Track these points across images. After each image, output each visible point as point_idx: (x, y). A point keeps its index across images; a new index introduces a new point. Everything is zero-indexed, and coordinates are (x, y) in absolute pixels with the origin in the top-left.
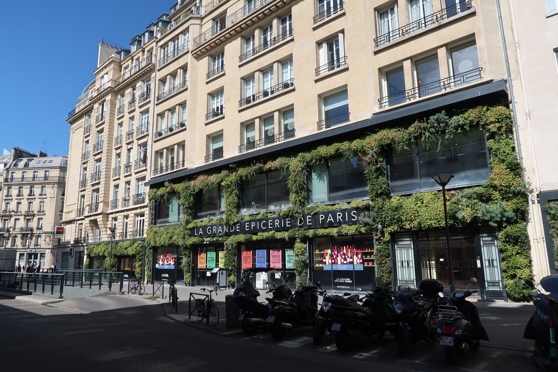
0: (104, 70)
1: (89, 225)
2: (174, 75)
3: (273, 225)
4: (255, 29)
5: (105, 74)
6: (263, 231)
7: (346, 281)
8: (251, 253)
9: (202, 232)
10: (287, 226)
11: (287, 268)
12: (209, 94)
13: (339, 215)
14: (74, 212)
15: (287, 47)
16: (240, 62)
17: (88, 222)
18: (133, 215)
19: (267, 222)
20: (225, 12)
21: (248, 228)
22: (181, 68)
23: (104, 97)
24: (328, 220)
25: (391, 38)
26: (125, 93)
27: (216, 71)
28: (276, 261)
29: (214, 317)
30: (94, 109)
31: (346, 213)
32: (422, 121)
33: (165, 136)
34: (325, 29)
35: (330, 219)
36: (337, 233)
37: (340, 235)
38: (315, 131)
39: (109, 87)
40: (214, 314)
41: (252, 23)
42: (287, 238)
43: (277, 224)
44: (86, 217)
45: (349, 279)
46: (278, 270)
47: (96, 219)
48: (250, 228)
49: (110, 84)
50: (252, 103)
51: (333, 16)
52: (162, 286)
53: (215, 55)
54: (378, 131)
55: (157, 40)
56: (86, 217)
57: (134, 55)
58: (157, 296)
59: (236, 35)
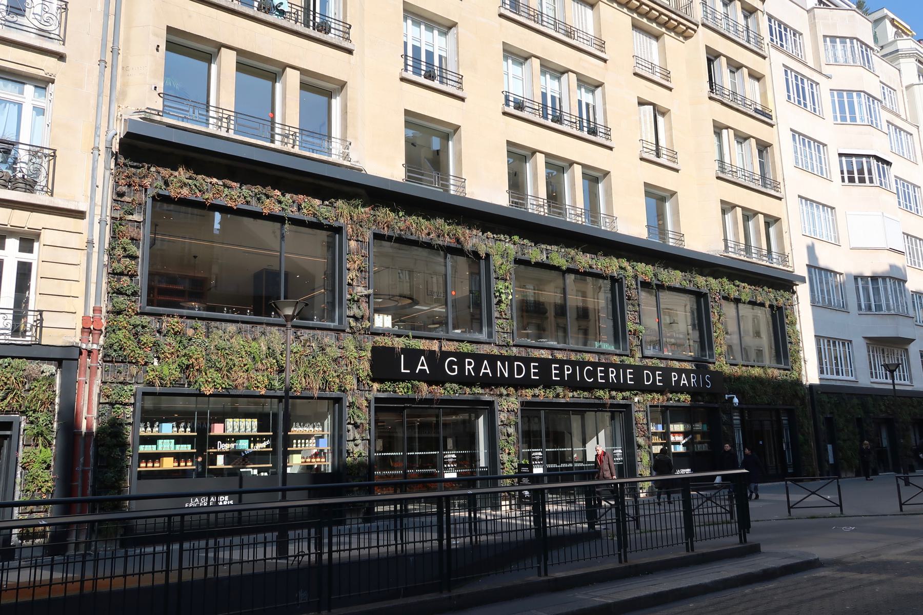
9: (686, 382)
10: (403, 371)
19: (595, 371)
21: (556, 375)
24: (419, 367)
43: (470, 367)
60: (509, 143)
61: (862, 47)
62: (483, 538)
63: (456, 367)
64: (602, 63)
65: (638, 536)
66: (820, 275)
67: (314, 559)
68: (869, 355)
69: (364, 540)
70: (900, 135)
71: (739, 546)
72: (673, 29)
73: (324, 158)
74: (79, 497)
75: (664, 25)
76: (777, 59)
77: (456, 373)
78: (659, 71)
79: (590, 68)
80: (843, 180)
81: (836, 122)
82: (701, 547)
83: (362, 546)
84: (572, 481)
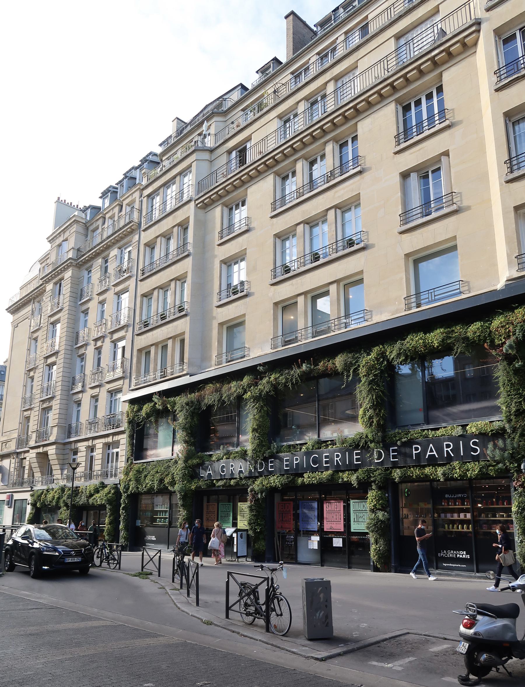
0: (62, 236)
1: (35, 460)
2: (167, 236)
4: (296, 161)
5: (63, 241)
6: (314, 470)
7: (458, 556)
8: (341, 505)
11: (352, 530)
12: (277, 236)
13: (338, 456)
14: (14, 441)
15: (351, 184)
16: (274, 211)
17: (34, 455)
18: (101, 446)
20: (249, 139)
22: (179, 225)
23: (61, 273)
24: (428, 453)
25: (515, 167)
26: (109, 256)
27: (351, 164)
28: (334, 520)
29: (279, 617)
30: (47, 291)
31: (461, 442)
33: (154, 326)
34: (414, 152)
35: (432, 451)
37: (448, 479)
38: (400, 312)
39: (70, 259)
40: (279, 613)
41: (257, 174)
42: (355, 484)
44: (32, 448)
45: (465, 552)
46: (338, 534)
47: (47, 451)
49: (70, 255)
50: (240, 295)
51: (427, 133)
52: (159, 554)
54: (517, 308)
55: (142, 188)
56: (32, 448)
57: (107, 211)
58: (148, 571)
59: (265, 171)
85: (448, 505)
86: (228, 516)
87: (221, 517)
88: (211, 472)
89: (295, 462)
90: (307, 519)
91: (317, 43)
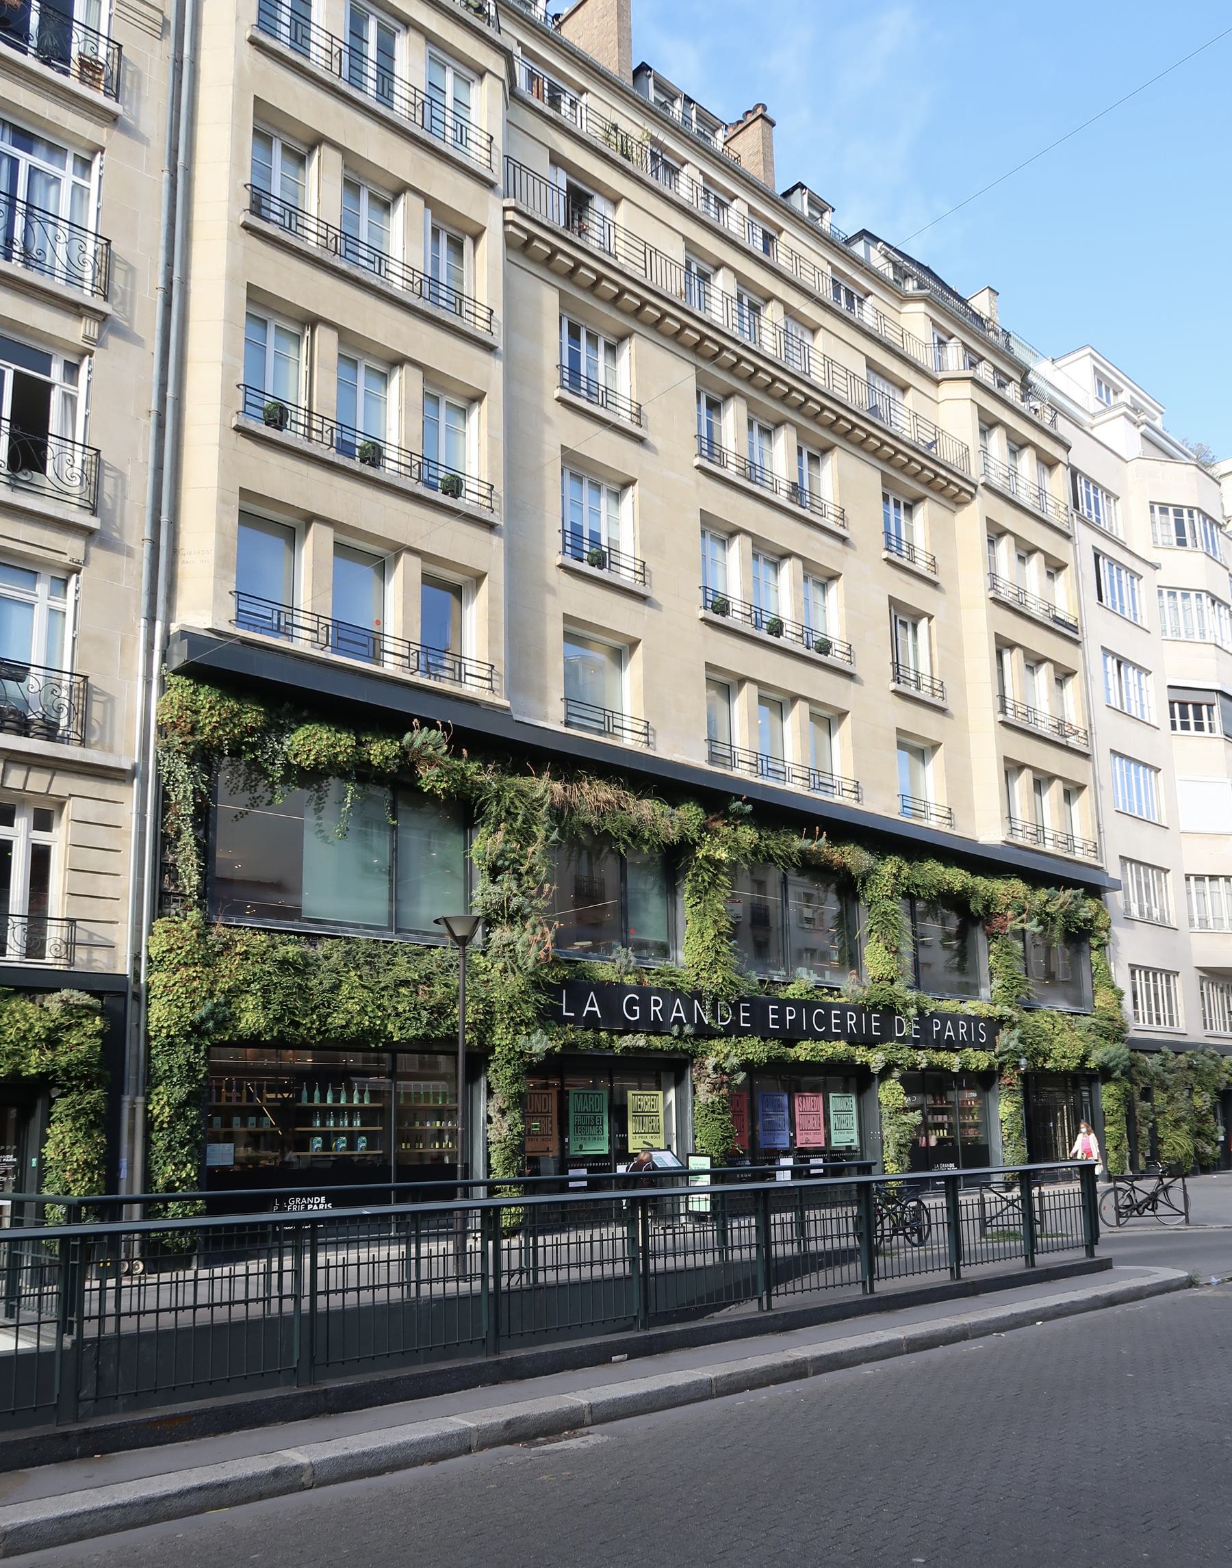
3: (842, 1025)
6: (818, 1037)
9: (952, 1034)
10: (565, 1014)
21: (775, 1022)
24: (587, 1008)
32: (465, 752)
36: (196, 1030)
43: (657, 1009)
48: (780, 1021)
53: (366, 179)
60: (709, 666)
61: (1205, 522)
62: (660, 1263)
63: (638, 1008)
64: (838, 545)
65: (916, 1254)
66: (1138, 872)
67: (308, 1307)
68: (1202, 993)
69: (221, 1292)
70: (1119, 576)
71: (1025, 1271)
72: (941, 491)
73: (446, 686)
74: (459, 1181)
75: (929, 483)
76: (1086, 538)
77: (638, 1017)
78: (733, 461)
79: (822, 550)
80: (1174, 727)
81: (1164, 637)
82: (970, 1273)
83: (217, 1300)
84: (388, 1202)
85: (935, 1104)
86: (597, 1123)
87: (577, 1125)
88: (952, 1034)
89: (788, 1018)
90: (772, 1129)
91: (712, 158)
